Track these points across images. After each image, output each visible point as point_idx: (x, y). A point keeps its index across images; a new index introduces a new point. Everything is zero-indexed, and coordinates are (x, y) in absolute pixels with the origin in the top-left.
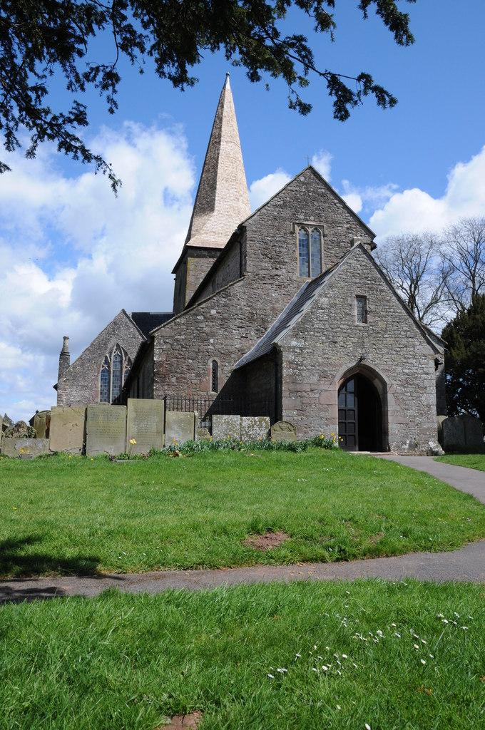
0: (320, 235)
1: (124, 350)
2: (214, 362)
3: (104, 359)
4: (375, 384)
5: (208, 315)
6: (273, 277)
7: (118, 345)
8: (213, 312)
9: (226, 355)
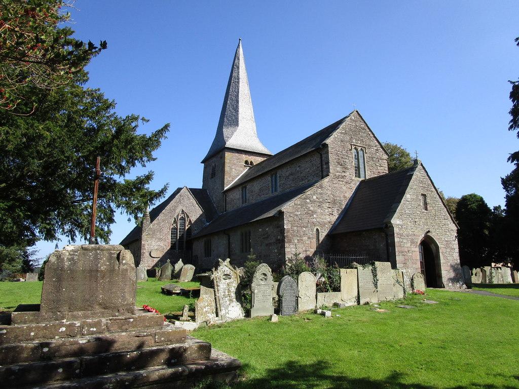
0: (363, 153)
1: (186, 214)
2: (317, 230)
3: (174, 220)
4: (432, 247)
5: (312, 199)
6: (343, 177)
7: (183, 211)
8: (315, 197)
9: (323, 225)
